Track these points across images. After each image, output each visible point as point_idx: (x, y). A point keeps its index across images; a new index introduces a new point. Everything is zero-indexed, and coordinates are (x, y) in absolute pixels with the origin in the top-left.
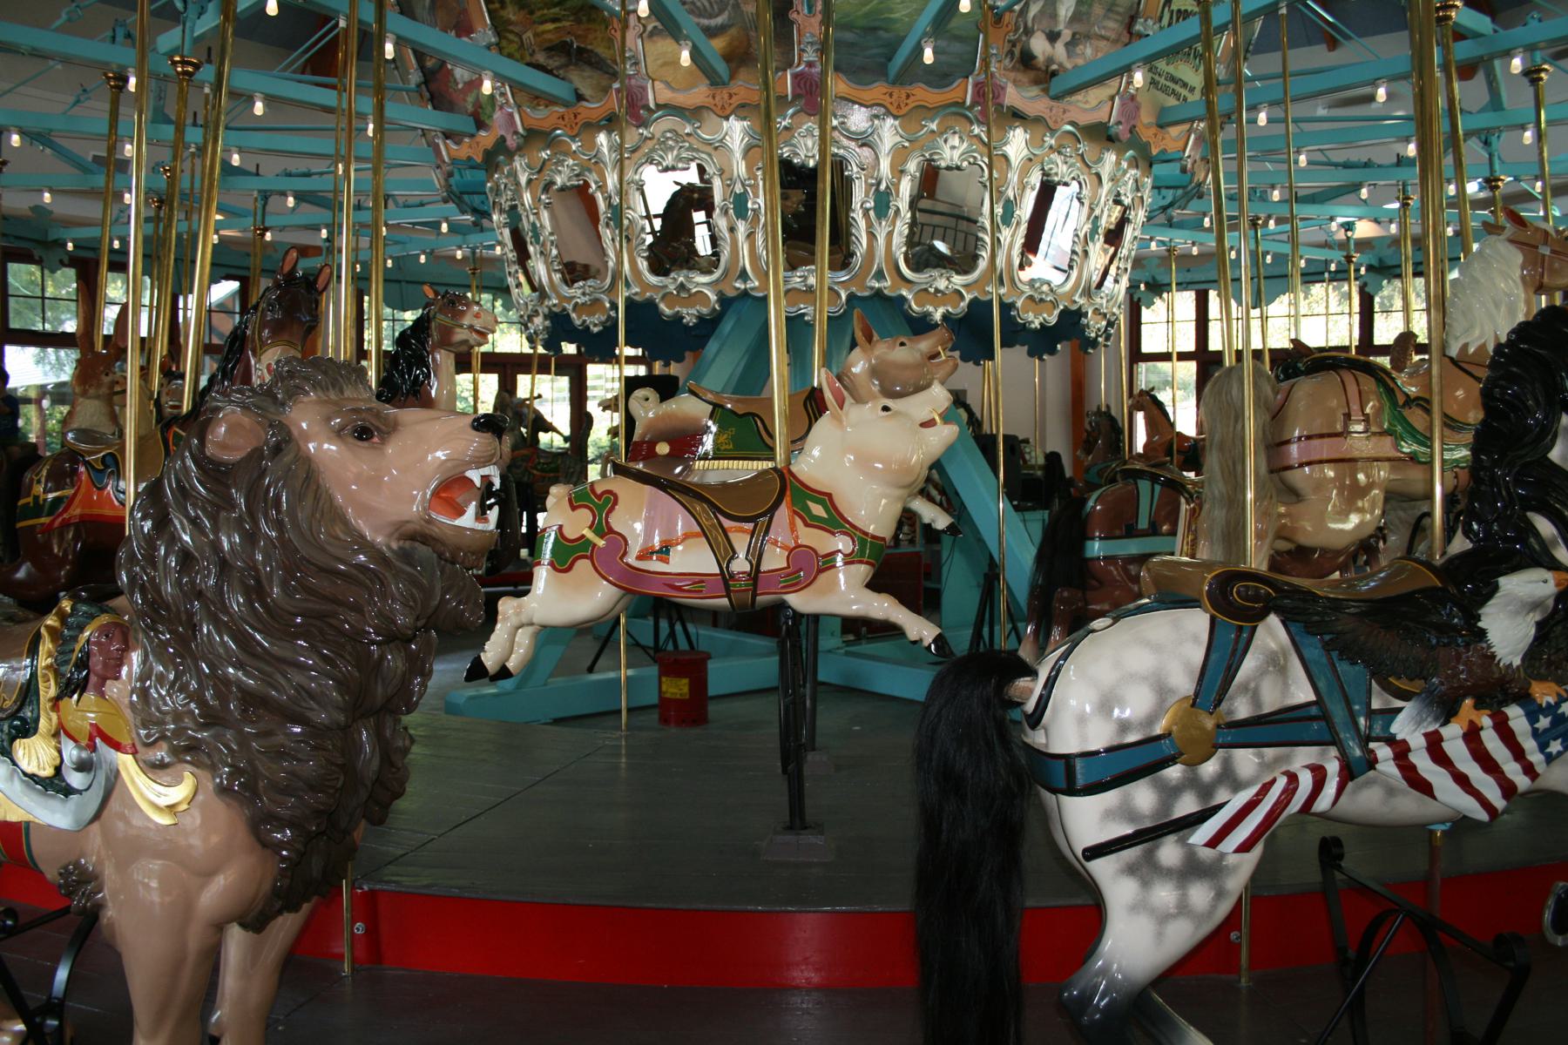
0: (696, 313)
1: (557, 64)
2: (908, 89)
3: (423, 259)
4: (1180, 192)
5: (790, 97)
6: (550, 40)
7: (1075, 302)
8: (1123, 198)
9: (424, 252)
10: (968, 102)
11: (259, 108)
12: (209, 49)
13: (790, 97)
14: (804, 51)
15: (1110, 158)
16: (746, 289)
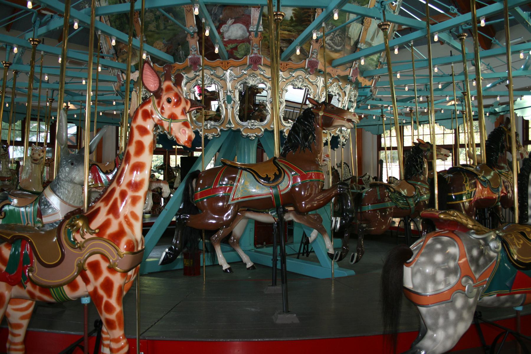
1: (284, 45)
2: (287, 62)
4: (363, 98)
6: (284, 37)
7: (336, 133)
10: (306, 67)
14: (253, 49)
15: (349, 86)
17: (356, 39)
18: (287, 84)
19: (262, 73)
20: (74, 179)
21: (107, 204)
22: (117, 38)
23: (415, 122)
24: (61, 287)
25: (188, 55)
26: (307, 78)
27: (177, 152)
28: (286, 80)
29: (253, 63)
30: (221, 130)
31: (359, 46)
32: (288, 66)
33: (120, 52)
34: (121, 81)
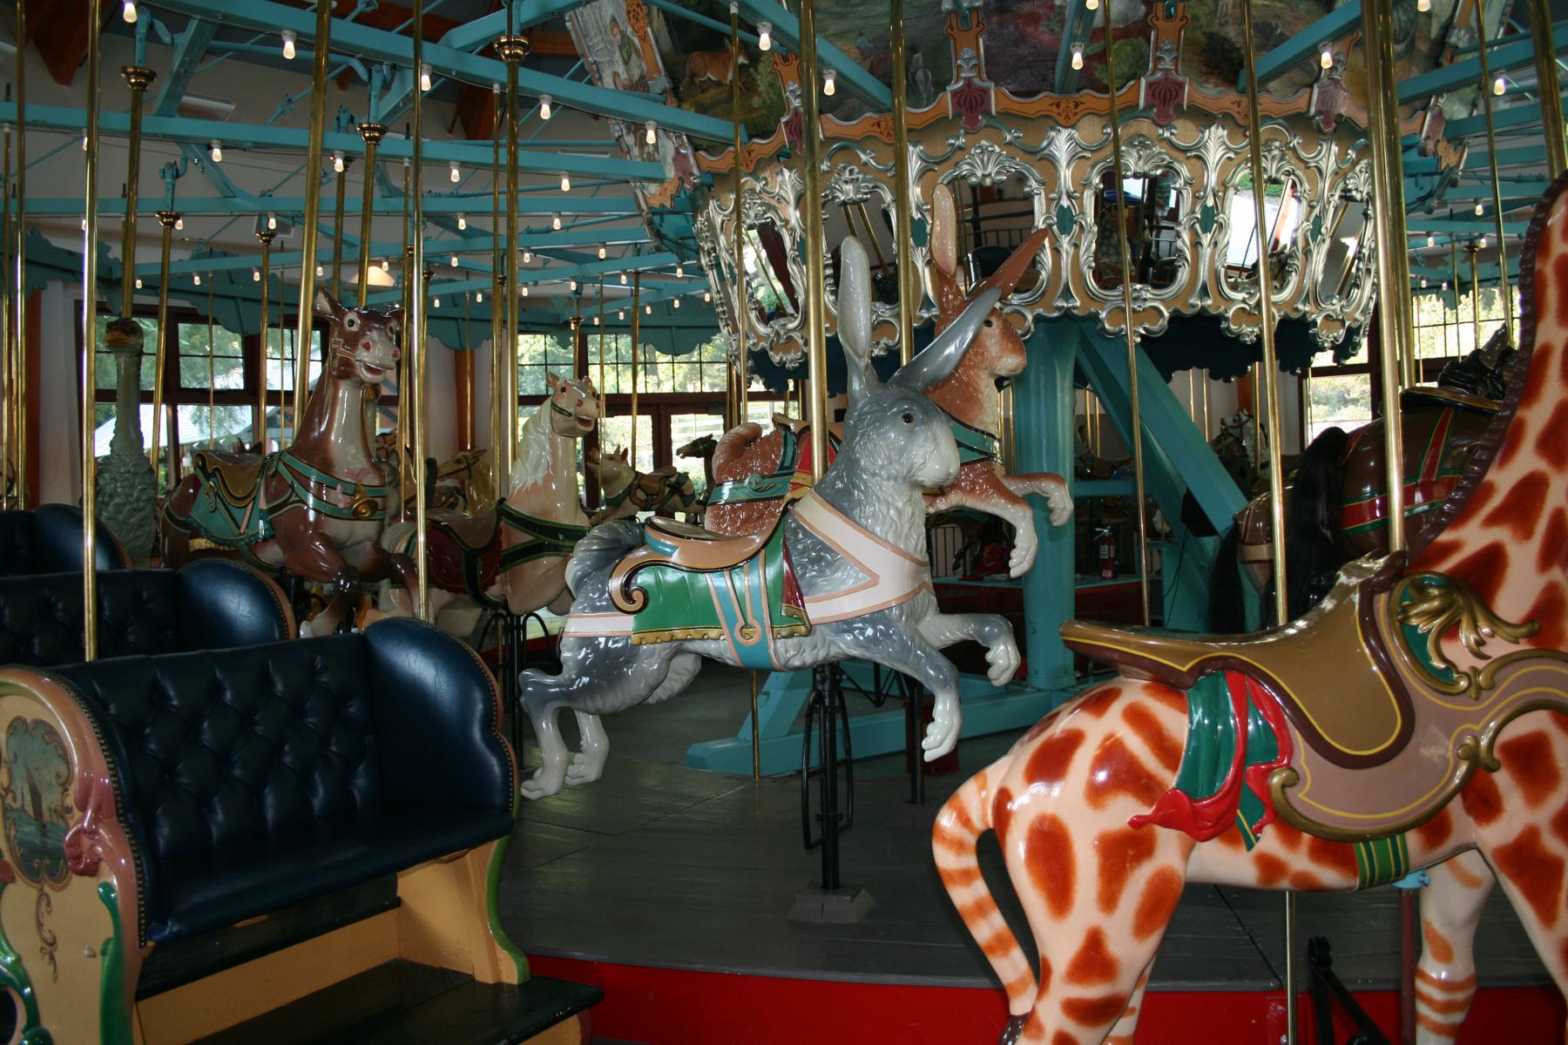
0: (1143, 332)
3: (677, 304)
4: (1437, 178)
5: (951, 117)
7: (1297, 310)
8: (1354, 193)
9: (677, 297)
11: (455, 175)
12: (408, 125)
13: (951, 117)
16: (930, 318)
17: (1445, 17)
18: (1238, 166)
19: (1167, 134)
20: (919, 470)
21: (1527, 534)
22: (554, 97)
23: (1451, 285)
24: (1398, 837)
25: (948, 82)
26: (1294, 149)
27: (639, 406)
28: (1236, 153)
29: (1158, 101)
30: (1038, 319)
31: (1453, 39)
32: (1081, 107)
33: (692, 82)
34: (692, 174)
